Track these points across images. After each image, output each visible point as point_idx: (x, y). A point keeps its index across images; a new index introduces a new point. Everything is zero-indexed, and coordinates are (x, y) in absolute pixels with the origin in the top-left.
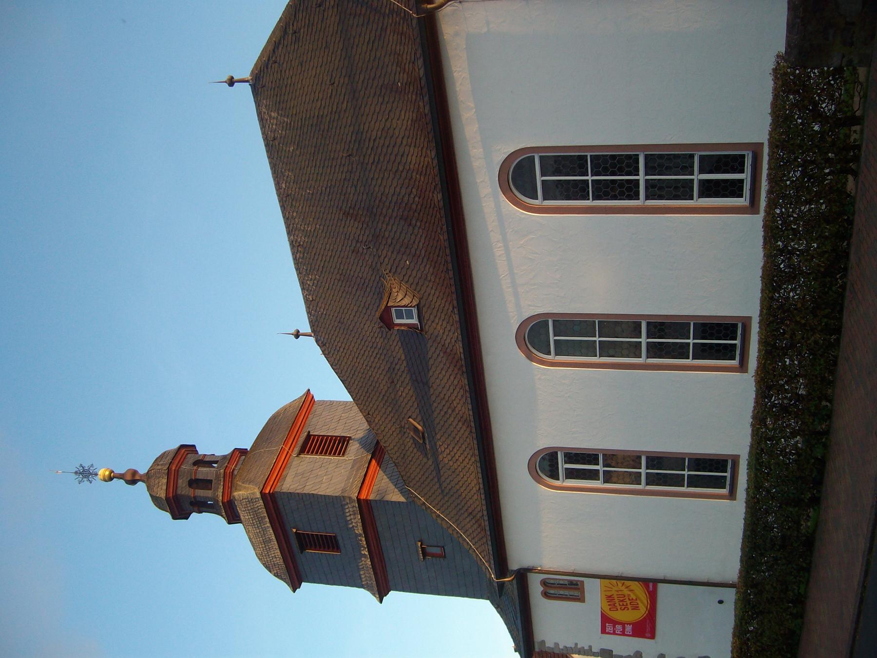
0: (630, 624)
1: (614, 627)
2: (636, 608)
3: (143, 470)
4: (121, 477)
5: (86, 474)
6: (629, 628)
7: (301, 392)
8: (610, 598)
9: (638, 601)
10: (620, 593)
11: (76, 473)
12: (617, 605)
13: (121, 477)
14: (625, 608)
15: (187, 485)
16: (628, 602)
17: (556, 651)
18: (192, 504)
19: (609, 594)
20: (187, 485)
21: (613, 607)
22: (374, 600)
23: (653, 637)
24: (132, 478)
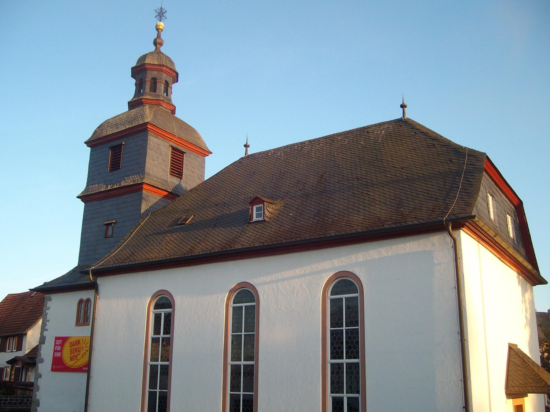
0: (61, 355)
1: (60, 345)
2: (71, 359)
3: (163, 49)
4: (159, 36)
5: (161, 14)
6: (59, 354)
8: (78, 342)
9: (76, 361)
10: (81, 349)
11: (161, 8)
12: (74, 347)
13: (159, 36)
14: (72, 352)
15: (152, 77)
16: (75, 354)
17: (44, 308)
18: (141, 80)
19: (81, 342)
20: (152, 77)
21: (72, 344)
22: (79, 193)
23: (53, 370)
24: (157, 43)
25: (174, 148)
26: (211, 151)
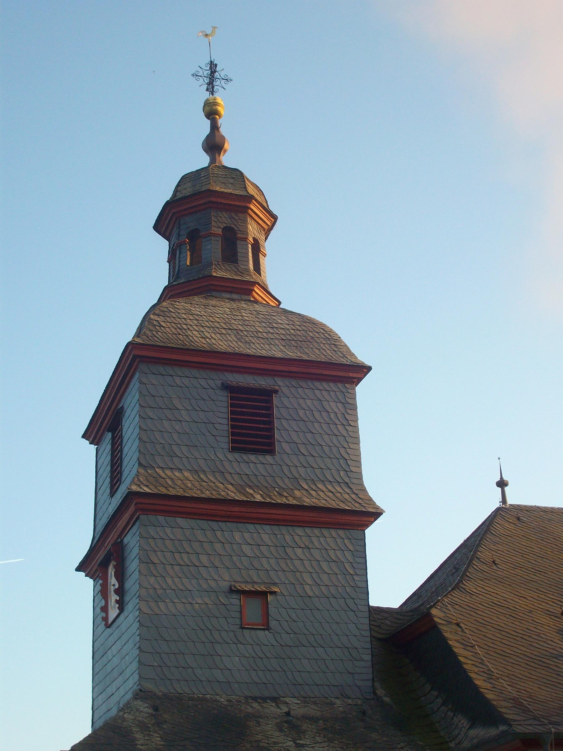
3: (228, 160)
7: (362, 355)
11: (211, 62)
13: (215, 127)
15: (211, 224)
20: (211, 224)
24: (214, 145)
25: (226, 387)
26: (368, 363)
